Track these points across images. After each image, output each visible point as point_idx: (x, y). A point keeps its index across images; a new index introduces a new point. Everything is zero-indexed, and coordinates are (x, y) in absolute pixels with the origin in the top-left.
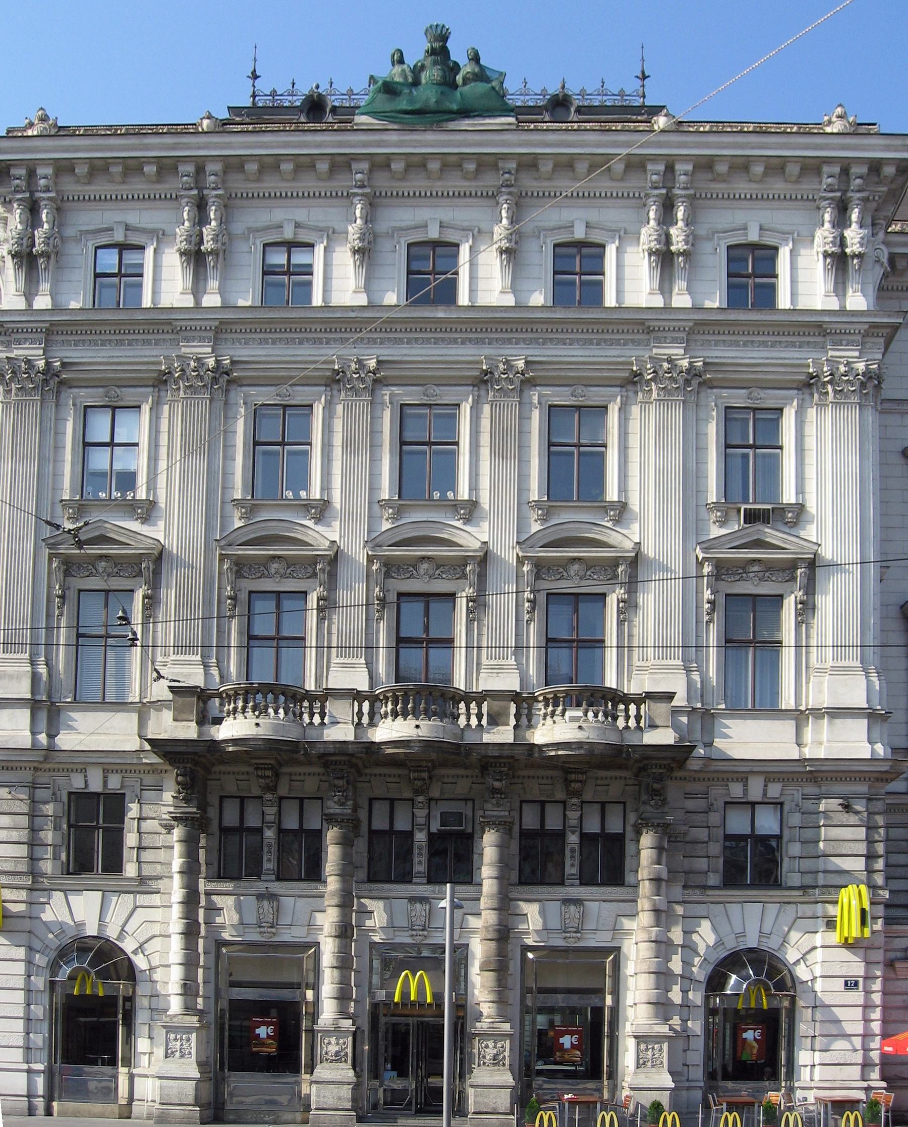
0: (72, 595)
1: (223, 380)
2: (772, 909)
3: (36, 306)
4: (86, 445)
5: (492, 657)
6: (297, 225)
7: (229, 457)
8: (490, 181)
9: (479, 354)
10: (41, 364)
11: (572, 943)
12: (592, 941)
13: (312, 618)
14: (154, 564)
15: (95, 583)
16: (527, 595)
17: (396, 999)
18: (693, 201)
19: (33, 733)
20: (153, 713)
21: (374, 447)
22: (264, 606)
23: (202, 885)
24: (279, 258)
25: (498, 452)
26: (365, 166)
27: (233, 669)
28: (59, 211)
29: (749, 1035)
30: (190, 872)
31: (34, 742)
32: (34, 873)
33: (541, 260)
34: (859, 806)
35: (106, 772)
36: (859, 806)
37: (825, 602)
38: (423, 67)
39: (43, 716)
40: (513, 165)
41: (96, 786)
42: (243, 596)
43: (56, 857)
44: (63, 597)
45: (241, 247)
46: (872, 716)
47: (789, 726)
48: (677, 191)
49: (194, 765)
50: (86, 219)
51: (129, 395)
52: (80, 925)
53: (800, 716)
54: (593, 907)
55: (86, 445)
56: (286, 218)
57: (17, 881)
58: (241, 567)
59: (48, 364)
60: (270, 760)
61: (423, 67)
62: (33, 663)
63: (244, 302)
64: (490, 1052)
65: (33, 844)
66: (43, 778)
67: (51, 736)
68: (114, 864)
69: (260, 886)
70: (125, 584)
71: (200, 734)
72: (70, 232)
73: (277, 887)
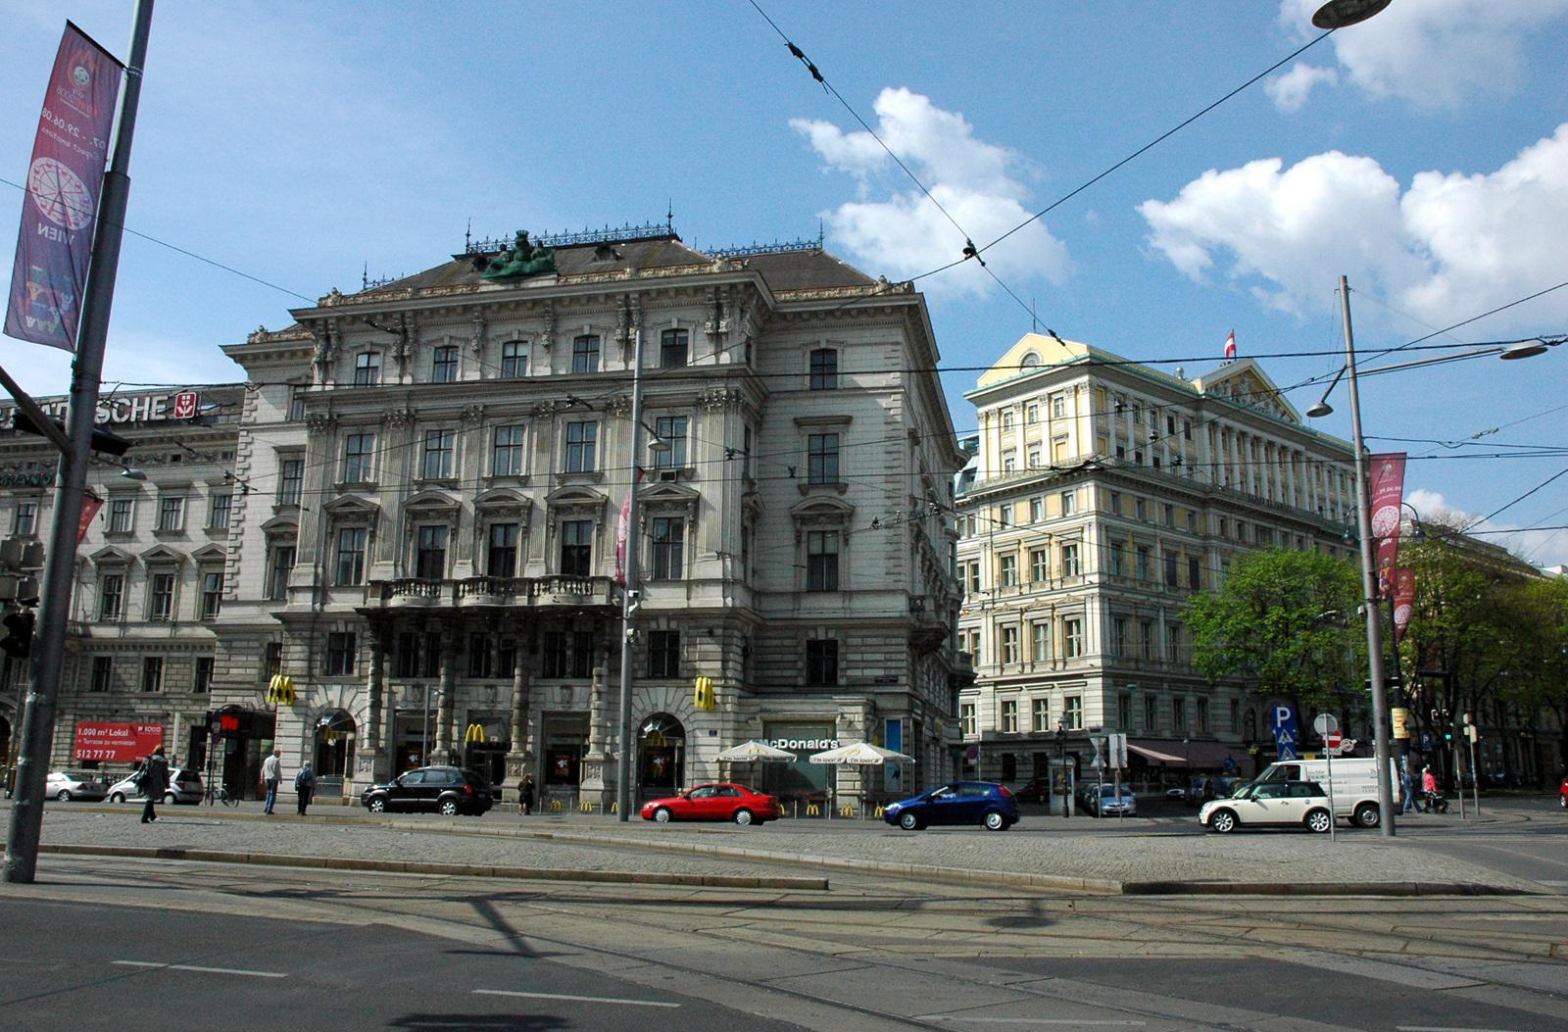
0: (337, 533)
1: (412, 420)
2: (672, 691)
3: (404, 382)
4: (496, 446)
5: (535, 561)
6: (451, 338)
7: (413, 458)
8: (539, 310)
9: (700, 389)
10: (327, 417)
11: (566, 710)
12: (576, 709)
13: (594, 534)
14: (373, 515)
15: (349, 525)
16: (551, 524)
17: (482, 740)
18: (642, 313)
19: (314, 603)
20: (694, 587)
21: (482, 449)
22: (573, 529)
23: (385, 681)
24: (510, 352)
25: (541, 449)
26: (479, 308)
27: (480, 567)
28: (340, 338)
29: (658, 761)
30: (378, 674)
31: (314, 609)
32: (310, 675)
33: (566, 346)
34: (719, 632)
35: (346, 623)
36: (719, 632)
37: (703, 525)
38: (515, 252)
39: (319, 595)
40: (549, 302)
41: (342, 629)
42: (560, 525)
43: (321, 666)
44: (332, 533)
45: (492, 345)
46: (724, 582)
47: (683, 591)
48: (632, 308)
49: (379, 621)
50: (496, 330)
51: (369, 429)
52: (330, 703)
53: (690, 584)
54: (577, 690)
55: (427, 450)
56: (513, 330)
57: (301, 680)
58: (414, 515)
59: (331, 416)
60: (419, 617)
61: (515, 252)
62: (316, 567)
63: (562, 372)
64: (514, 768)
65: (310, 660)
66: (317, 626)
67: (322, 604)
68: (350, 670)
69: (414, 681)
70: (361, 525)
71: (382, 604)
72: (345, 347)
73: (423, 681)
